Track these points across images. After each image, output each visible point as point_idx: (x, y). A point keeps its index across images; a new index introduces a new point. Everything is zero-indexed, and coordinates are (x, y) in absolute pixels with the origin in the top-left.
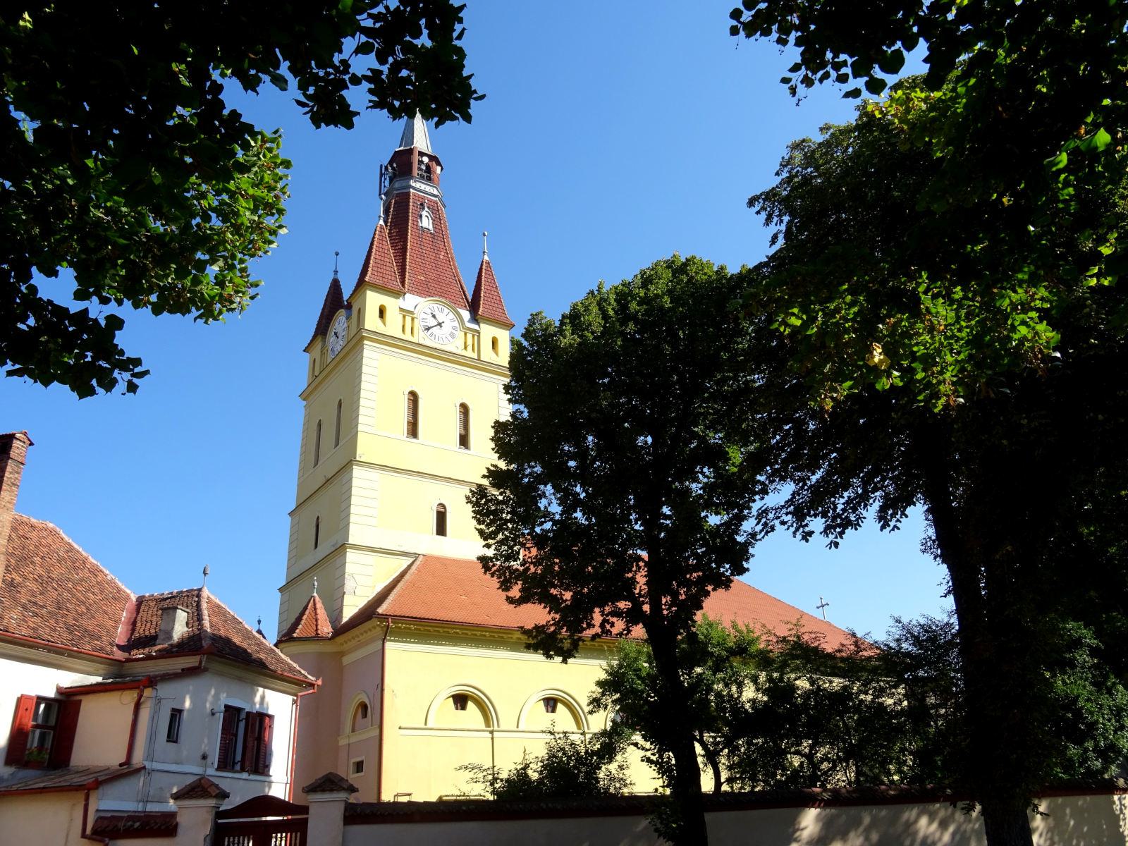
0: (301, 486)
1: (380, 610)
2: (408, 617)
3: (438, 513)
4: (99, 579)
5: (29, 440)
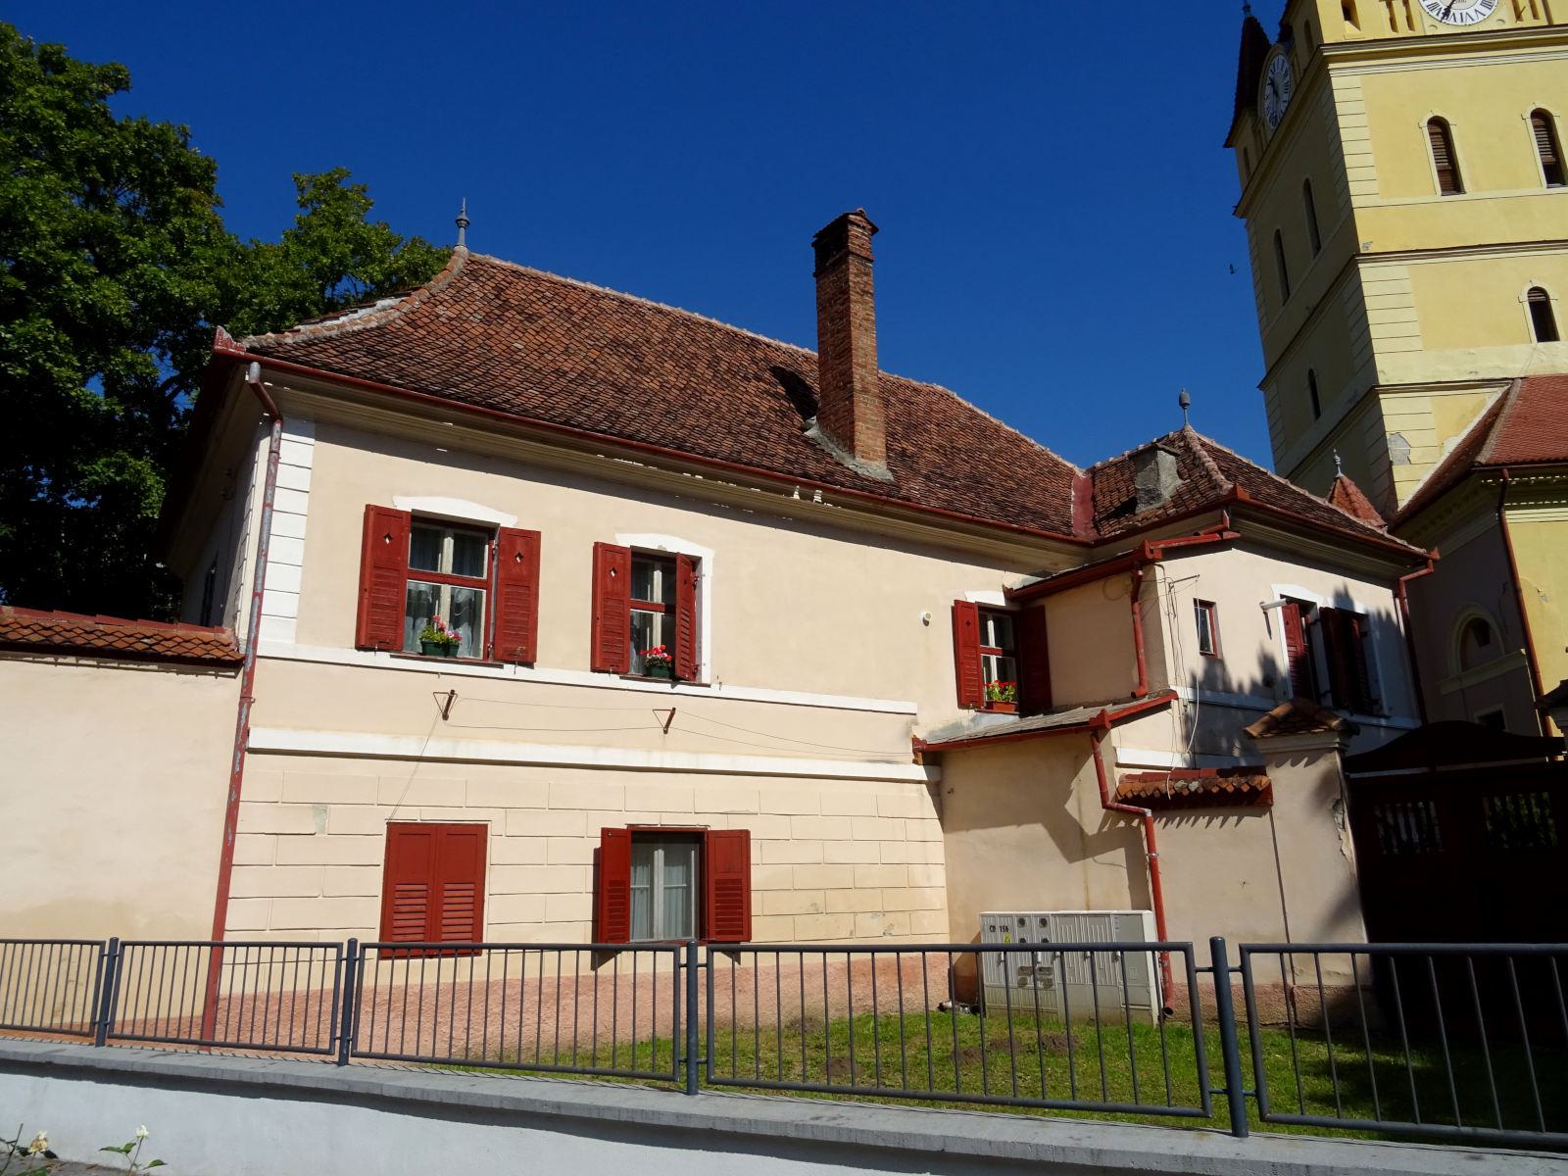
0: (1266, 362)
1: (1484, 457)
2: (1540, 461)
3: (1533, 305)
4: (1024, 450)
5: (870, 224)
